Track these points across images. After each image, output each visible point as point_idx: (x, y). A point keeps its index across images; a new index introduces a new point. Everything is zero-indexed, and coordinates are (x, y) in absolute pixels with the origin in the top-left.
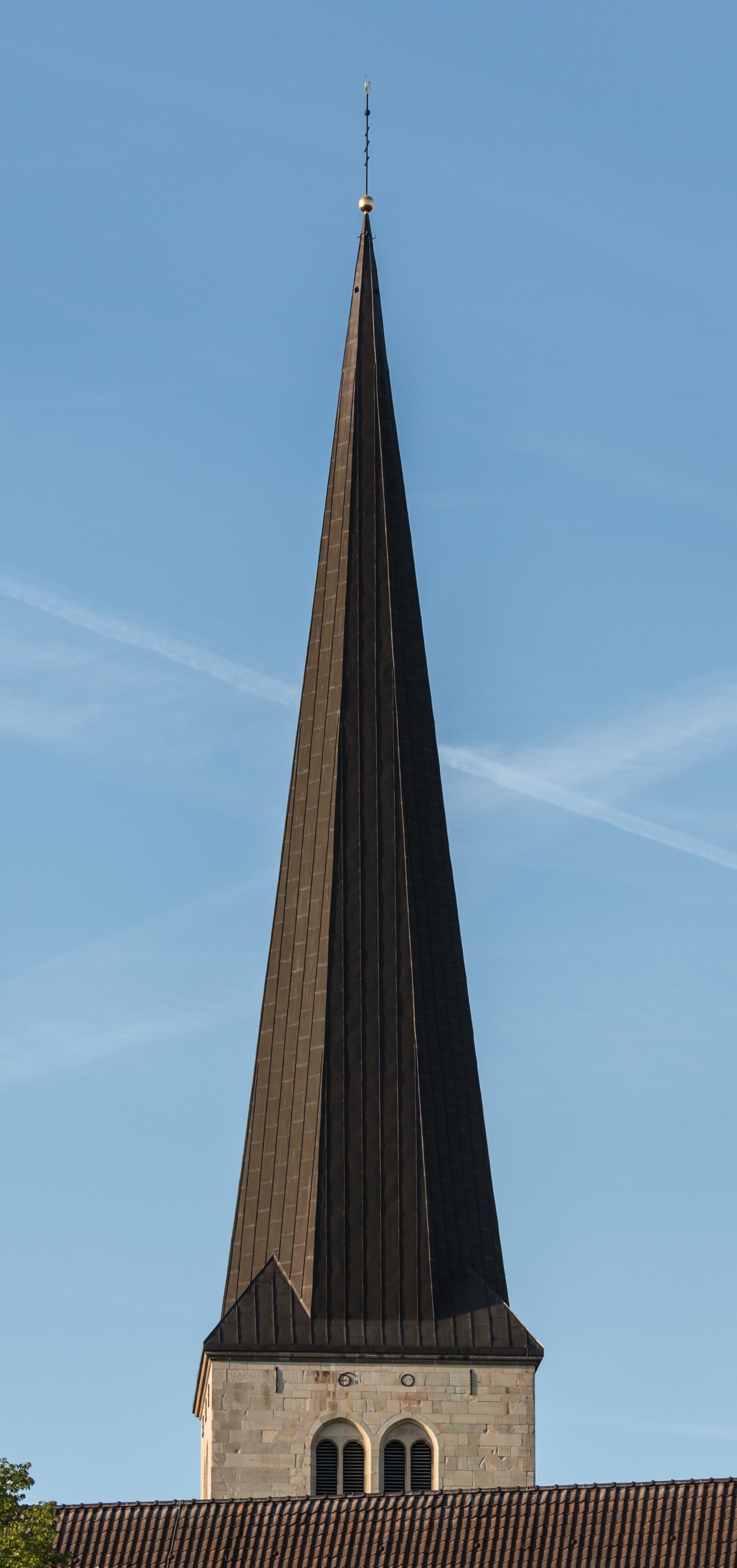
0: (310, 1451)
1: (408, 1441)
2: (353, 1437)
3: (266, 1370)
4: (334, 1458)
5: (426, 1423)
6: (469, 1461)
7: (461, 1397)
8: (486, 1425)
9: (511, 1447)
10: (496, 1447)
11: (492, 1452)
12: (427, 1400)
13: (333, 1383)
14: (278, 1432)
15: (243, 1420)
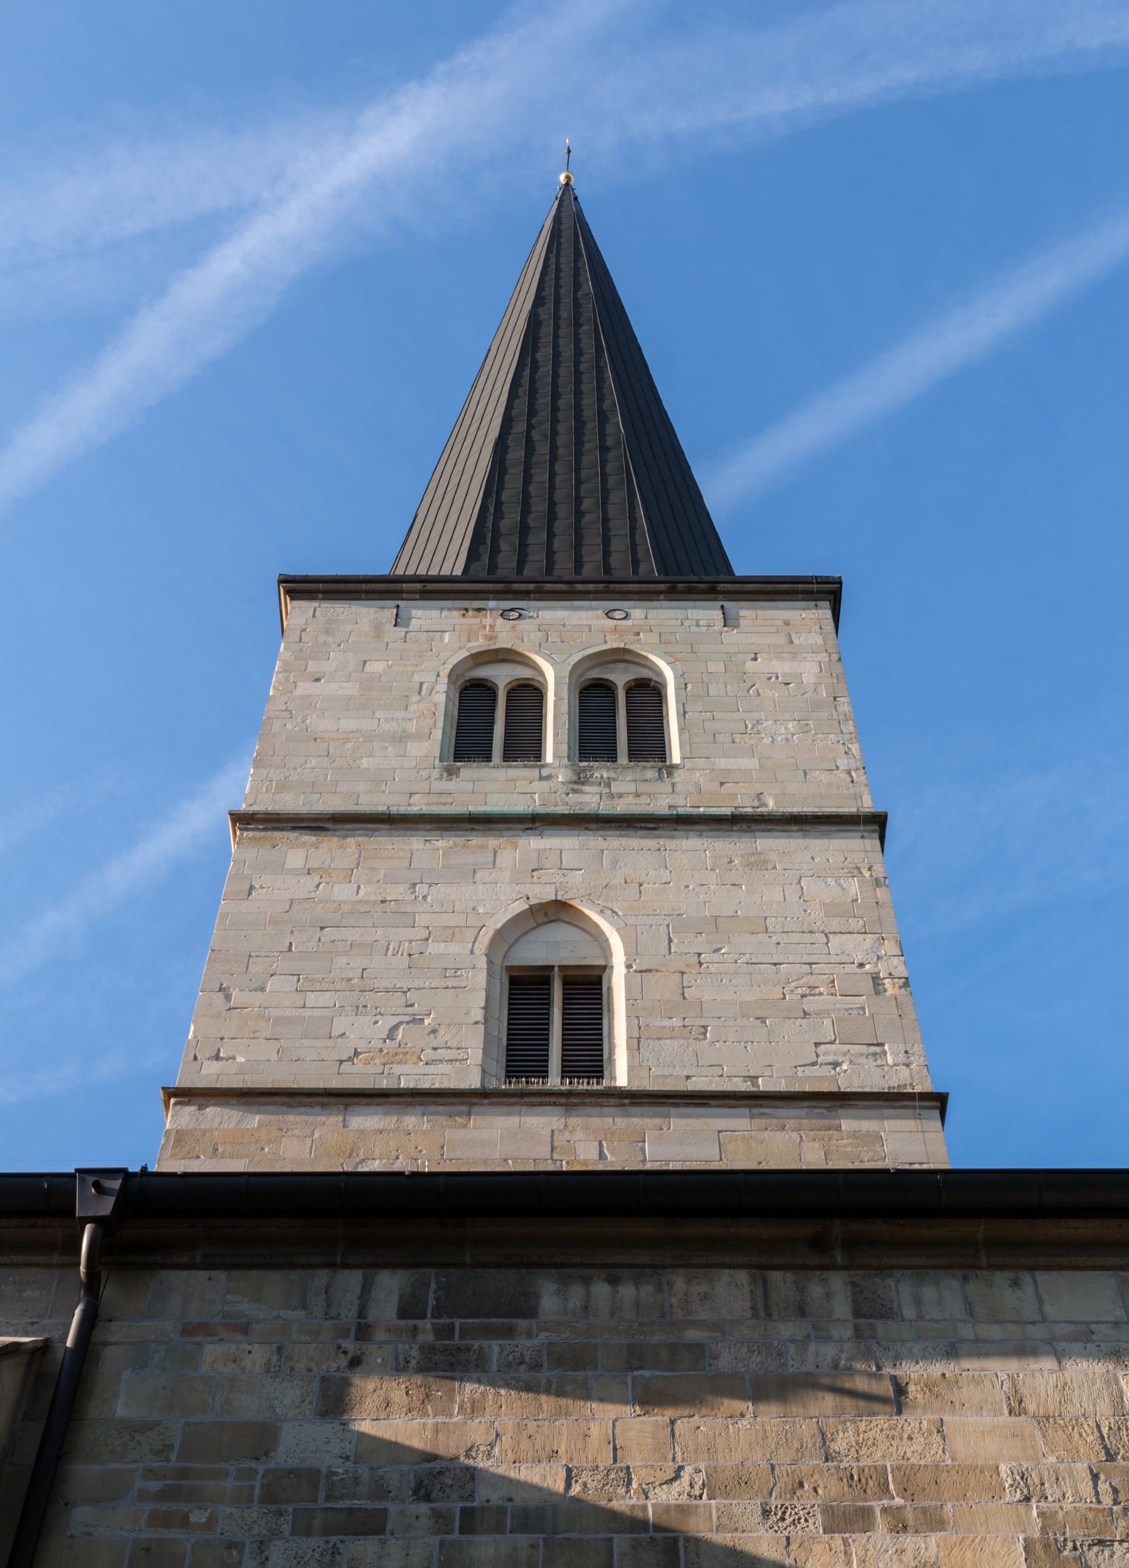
0: (446, 680)
1: (620, 678)
2: (523, 673)
3: (608, 1539)
4: (566, 1063)
5: (651, 653)
6: (728, 687)
7: (708, 629)
8: (755, 654)
9: (801, 674)
10: (775, 675)
11: (770, 678)
12: (651, 631)
13: (491, 617)
14: (513, 1162)
15: (334, 652)
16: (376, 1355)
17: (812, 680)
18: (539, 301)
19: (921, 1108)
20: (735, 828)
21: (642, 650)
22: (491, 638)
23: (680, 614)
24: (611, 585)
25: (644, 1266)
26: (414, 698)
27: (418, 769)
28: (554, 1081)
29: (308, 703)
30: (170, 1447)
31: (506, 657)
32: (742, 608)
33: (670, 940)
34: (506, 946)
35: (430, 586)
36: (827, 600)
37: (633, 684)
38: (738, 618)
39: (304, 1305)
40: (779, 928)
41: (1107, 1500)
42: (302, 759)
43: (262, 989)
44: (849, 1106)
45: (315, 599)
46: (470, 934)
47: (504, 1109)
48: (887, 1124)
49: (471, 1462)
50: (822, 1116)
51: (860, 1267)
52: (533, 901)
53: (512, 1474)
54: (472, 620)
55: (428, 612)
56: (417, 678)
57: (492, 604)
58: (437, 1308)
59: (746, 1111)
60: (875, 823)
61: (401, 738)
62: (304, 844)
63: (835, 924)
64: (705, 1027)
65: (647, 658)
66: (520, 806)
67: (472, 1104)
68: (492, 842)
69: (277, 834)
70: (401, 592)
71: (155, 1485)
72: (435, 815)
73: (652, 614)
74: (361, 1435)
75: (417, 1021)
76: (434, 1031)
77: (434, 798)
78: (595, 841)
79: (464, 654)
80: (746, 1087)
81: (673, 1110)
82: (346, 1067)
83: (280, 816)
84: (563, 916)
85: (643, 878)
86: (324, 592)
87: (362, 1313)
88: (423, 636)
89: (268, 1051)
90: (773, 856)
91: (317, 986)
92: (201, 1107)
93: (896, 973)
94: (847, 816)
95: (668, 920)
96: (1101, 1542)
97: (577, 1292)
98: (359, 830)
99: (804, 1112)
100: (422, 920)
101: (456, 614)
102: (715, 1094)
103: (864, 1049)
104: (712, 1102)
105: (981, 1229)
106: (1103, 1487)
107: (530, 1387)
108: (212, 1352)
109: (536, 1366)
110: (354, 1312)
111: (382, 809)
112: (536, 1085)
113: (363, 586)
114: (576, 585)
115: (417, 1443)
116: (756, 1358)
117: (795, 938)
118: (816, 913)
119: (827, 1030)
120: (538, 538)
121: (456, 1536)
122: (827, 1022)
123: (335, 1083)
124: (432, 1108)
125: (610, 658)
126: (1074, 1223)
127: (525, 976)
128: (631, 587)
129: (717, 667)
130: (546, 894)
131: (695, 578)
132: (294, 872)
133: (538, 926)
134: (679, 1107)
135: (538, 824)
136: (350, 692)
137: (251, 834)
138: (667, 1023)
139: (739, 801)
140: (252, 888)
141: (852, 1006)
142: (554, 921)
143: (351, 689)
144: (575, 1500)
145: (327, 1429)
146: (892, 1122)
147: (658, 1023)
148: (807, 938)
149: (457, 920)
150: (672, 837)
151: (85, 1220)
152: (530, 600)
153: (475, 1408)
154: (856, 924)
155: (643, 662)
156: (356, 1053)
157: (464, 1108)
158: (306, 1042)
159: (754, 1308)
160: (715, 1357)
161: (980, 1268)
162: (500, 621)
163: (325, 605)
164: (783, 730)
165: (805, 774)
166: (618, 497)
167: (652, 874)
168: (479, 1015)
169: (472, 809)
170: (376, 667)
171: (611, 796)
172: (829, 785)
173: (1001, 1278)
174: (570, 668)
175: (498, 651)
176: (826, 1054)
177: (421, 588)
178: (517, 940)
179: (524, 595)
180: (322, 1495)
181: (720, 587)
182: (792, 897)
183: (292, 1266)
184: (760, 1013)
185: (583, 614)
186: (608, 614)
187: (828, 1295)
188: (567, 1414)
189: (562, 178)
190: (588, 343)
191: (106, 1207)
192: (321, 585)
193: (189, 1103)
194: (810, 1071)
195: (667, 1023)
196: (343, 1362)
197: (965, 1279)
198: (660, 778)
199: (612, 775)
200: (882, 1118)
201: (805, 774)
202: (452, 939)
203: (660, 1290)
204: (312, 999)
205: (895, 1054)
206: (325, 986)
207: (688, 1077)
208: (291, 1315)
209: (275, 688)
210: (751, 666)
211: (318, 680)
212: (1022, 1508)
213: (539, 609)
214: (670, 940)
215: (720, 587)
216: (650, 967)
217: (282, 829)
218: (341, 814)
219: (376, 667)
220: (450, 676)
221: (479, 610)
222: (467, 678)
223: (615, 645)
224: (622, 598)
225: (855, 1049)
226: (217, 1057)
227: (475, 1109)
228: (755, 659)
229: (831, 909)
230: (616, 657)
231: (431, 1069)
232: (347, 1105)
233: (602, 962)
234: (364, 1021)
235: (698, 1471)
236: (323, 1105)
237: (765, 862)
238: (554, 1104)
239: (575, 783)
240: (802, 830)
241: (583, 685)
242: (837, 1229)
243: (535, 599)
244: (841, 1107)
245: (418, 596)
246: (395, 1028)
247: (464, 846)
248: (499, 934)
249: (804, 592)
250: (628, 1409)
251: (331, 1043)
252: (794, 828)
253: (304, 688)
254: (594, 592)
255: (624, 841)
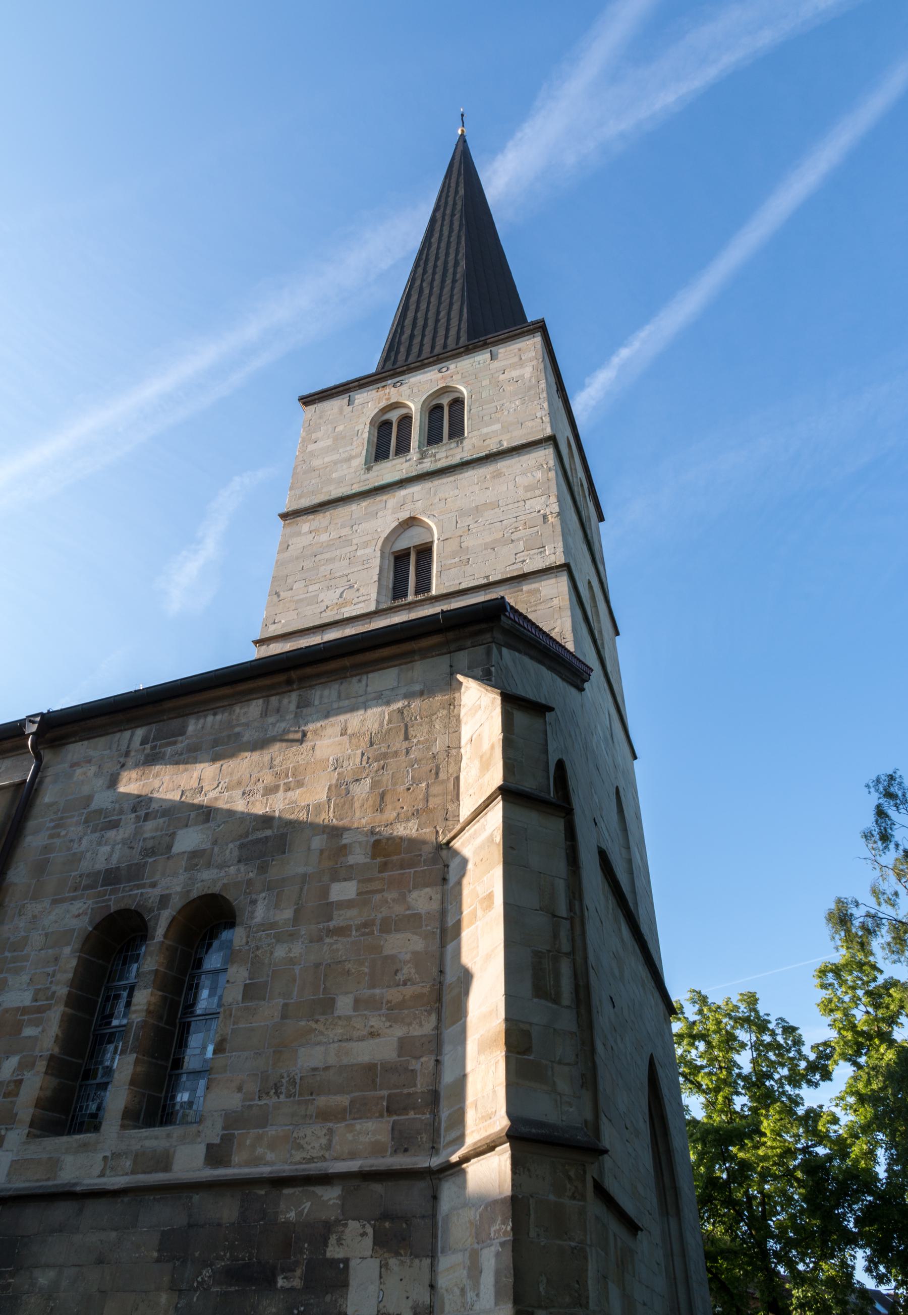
16: (130, 762)
17: (529, 376)
18: (435, 211)
19: (557, 572)
22: (388, 399)
23: (471, 360)
25: (226, 706)
26: (355, 439)
27: (355, 472)
28: (411, 598)
29: (312, 454)
30: (59, 810)
32: (499, 349)
33: (457, 522)
34: (391, 543)
35: (362, 382)
38: (498, 353)
39: (110, 748)
40: (504, 504)
41: (364, 763)
42: (308, 482)
43: (292, 589)
44: (527, 579)
45: (315, 403)
46: (374, 543)
47: (384, 617)
48: (543, 583)
49: (152, 795)
50: (515, 587)
51: (303, 688)
52: (400, 520)
53: (164, 797)
54: (381, 393)
55: (362, 395)
56: (357, 429)
57: (389, 382)
58: (153, 739)
59: (483, 592)
61: (349, 459)
62: (309, 520)
63: (529, 495)
64: (469, 559)
66: (396, 477)
67: (372, 618)
68: (385, 497)
69: (299, 519)
71: (52, 824)
73: (459, 364)
74: (119, 792)
75: (351, 587)
76: (358, 590)
77: (361, 484)
79: (377, 410)
80: (485, 581)
81: (453, 600)
82: (324, 614)
84: (415, 523)
85: (447, 496)
86: (318, 399)
87: (128, 747)
88: (360, 407)
89: (292, 615)
90: (504, 470)
91: (313, 582)
92: (268, 645)
93: (553, 511)
95: (457, 513)
96: (357, 780)
97: (202, 721)
99: (507, 587)
100: (354, 542)
101: (374, 392)
103: (536, 551)
105: (346, 662)
106: (365, 758)
107: (177, 763)
108: (79, 771)
109: (181, 754)
110: (126, 745)
111: (340, 495)
112: (402, 602)
113: (334, 391)
115: (136, 792)
116: (257, 734)
117: (510, 507)
118: (521, 491)
119: (521, 546)
120: (417, 340)
121: (141, 823)
122: (521, 542)
123: (317, 623)
124: (356, 623)
126: (381, 650)
129: (486, 382)
130: (404, 515)
131: (476, 341)
132: (305, 534)
136: (328, 444)
137: (288, 521)
138: (453, 561)
139: (491, 447)
140: (288, 546)
143: (329, 442)
144: (183, 802)
145: (109, 793)
146: (545, 582)
147: (449, 562)
148: (516, 505)
149: (369, 537)
150: (461, 473)
151: (29, 735)
153: (157, 775)
154: (538, 492)
156: (327, 607)
157: (369, 620)
158: (308, 608)
159: (261, 714)
160: (243, 737)
161: (347, 677)
162: (393, 389)
163: (320, 405)
164: (513, 406)
165: (522, 424)
166: (456, 307)
167: (452, 493)
168: (376, 578)
169: (377, 484)
170: (340, 428)
171: (436, 461)
172: (532, 427)
173: (355, 680)
174: (421, 403)
175: (392, 404)
176: (519, 557)
178: (396, 539)
179: (402, 373)
180: (102, 817)
181: (489, 341)
182: (511, 487)
183: (108, 734)
184: (492, 546)
185: (429, 374)
186: (440, 371)
187: (289, 702)
188: (188, 770)
189: (460, 132)
191: (34, 728)
193: (263, 645)
194: (512, 567)
195: (453, 561)
196: (119, 767)
197: (341, 683)
198: (458, 446)
199: (437, 450)
200: (541, 581)
201: (522, 424)
202: (367, 547)
203: (230, 714)
204: (311, 588)
205: (550, 550)
206: (316, 581)
207: (460, 583)
208: (105, 752)
209: (299, 451)
210: (502, 377)
211: (316, 442)
212: (332, 773)
213: (410, 378)
214: (457, 522)
215: (489, 341)
217: (300, 516)
219: (340, 428)
220: (371, 423)
221: (384, 387)
223: (441, 386)
225: (532, 552)
226: (274, 623)
227: (373, 619)
228: (504, 373)
229: (528, 489)
231: (356, 606)
232: (323, 631)
233: (431, 540)
234: (331, 592)
235: (225, 782)
236: (314, 633)
237: (501, 473)
238: (404, 610)
239: (421, 459)
242: (294, 674)
243: (408, 373)
246: (343, 592)
247: (374, 503)
248: (387, 539)
249: (527, 331)
250: (207, 764)
251: (317, 605)
252: (514, 453)
253: (311, 447)
254: (433, 362)
255: (440, 481)
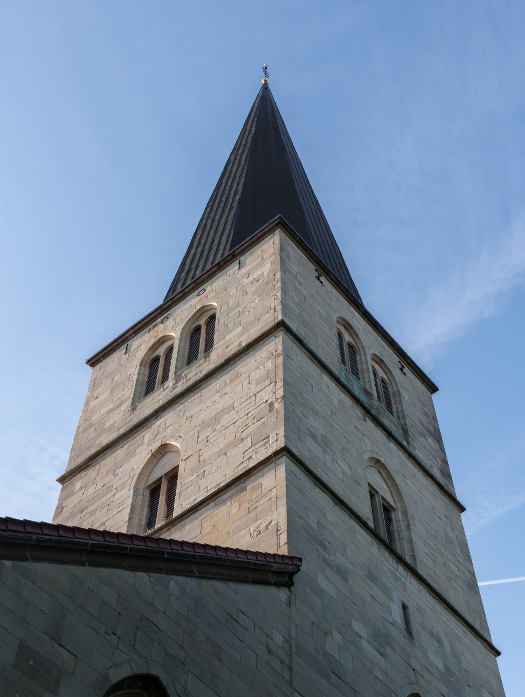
5: (211, 302)
20: (229, 366)
21: (208, 303)
24: (197, 281)
31: (163, 341)
36: (278, 228)
37: (209, 320)
60: (280, 327)
65: (210, 305)
70: (128, 337)
72: (122, 434)
78: (179, 408)
83: (73, 470)
94: (267, 331)
98: (100, 458)
102: (200, 503)
104: (200, 507)
113: (114, 345)
114: (185, 290)
125: (199, 314)
127: (156, 486)
128: (204, 276)
130: (156, 445)
133: (159, 460)
134: (189, 517)
135: (159, 414)
141: (260, 425)
142: (165, 454)
152: (172, 308)
154: (267, 382)
155: (210, 308)
177: (133, 331)
181: (236, 253)
190: (243, 162)
192: (100, 355)
215: (236, 253)
216: (188, 456)
218: (92, 456)
222: (151, 360)
224: (203, 283)
230: (201, 312)
240: (253, 349)
241: (191, 333)
243: (174, 307)
244: (248, 478)
245: (134, 335)
